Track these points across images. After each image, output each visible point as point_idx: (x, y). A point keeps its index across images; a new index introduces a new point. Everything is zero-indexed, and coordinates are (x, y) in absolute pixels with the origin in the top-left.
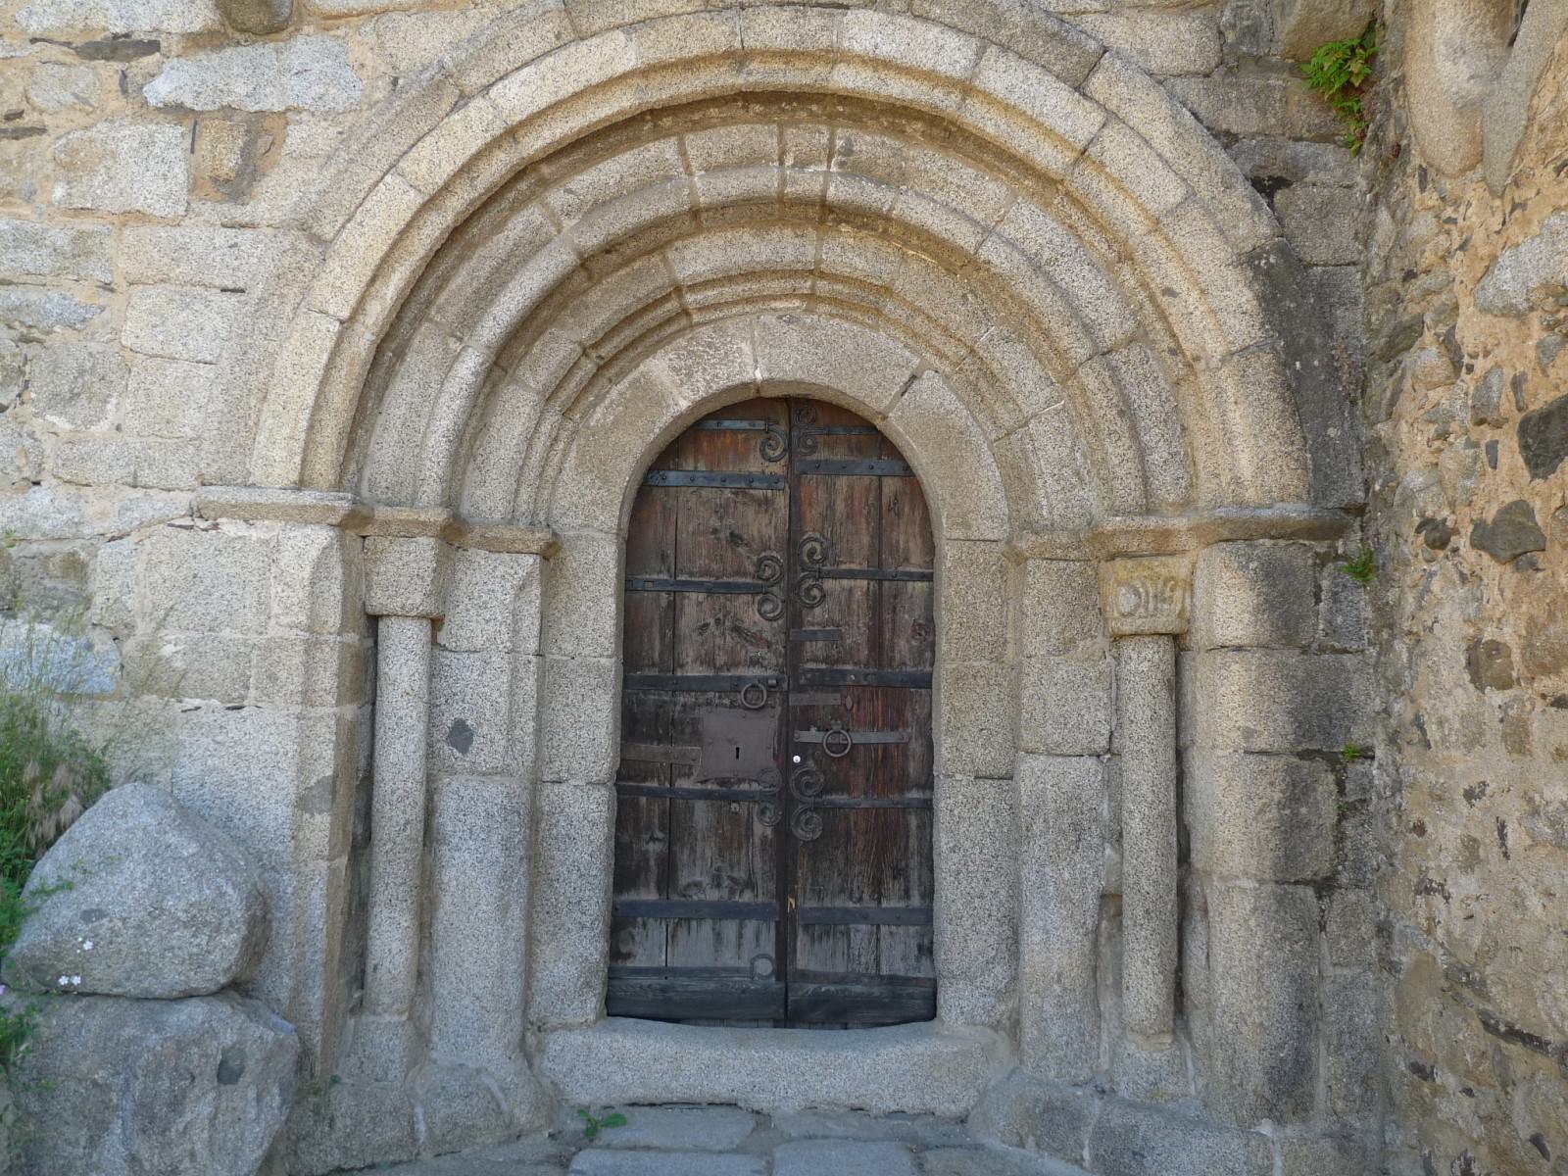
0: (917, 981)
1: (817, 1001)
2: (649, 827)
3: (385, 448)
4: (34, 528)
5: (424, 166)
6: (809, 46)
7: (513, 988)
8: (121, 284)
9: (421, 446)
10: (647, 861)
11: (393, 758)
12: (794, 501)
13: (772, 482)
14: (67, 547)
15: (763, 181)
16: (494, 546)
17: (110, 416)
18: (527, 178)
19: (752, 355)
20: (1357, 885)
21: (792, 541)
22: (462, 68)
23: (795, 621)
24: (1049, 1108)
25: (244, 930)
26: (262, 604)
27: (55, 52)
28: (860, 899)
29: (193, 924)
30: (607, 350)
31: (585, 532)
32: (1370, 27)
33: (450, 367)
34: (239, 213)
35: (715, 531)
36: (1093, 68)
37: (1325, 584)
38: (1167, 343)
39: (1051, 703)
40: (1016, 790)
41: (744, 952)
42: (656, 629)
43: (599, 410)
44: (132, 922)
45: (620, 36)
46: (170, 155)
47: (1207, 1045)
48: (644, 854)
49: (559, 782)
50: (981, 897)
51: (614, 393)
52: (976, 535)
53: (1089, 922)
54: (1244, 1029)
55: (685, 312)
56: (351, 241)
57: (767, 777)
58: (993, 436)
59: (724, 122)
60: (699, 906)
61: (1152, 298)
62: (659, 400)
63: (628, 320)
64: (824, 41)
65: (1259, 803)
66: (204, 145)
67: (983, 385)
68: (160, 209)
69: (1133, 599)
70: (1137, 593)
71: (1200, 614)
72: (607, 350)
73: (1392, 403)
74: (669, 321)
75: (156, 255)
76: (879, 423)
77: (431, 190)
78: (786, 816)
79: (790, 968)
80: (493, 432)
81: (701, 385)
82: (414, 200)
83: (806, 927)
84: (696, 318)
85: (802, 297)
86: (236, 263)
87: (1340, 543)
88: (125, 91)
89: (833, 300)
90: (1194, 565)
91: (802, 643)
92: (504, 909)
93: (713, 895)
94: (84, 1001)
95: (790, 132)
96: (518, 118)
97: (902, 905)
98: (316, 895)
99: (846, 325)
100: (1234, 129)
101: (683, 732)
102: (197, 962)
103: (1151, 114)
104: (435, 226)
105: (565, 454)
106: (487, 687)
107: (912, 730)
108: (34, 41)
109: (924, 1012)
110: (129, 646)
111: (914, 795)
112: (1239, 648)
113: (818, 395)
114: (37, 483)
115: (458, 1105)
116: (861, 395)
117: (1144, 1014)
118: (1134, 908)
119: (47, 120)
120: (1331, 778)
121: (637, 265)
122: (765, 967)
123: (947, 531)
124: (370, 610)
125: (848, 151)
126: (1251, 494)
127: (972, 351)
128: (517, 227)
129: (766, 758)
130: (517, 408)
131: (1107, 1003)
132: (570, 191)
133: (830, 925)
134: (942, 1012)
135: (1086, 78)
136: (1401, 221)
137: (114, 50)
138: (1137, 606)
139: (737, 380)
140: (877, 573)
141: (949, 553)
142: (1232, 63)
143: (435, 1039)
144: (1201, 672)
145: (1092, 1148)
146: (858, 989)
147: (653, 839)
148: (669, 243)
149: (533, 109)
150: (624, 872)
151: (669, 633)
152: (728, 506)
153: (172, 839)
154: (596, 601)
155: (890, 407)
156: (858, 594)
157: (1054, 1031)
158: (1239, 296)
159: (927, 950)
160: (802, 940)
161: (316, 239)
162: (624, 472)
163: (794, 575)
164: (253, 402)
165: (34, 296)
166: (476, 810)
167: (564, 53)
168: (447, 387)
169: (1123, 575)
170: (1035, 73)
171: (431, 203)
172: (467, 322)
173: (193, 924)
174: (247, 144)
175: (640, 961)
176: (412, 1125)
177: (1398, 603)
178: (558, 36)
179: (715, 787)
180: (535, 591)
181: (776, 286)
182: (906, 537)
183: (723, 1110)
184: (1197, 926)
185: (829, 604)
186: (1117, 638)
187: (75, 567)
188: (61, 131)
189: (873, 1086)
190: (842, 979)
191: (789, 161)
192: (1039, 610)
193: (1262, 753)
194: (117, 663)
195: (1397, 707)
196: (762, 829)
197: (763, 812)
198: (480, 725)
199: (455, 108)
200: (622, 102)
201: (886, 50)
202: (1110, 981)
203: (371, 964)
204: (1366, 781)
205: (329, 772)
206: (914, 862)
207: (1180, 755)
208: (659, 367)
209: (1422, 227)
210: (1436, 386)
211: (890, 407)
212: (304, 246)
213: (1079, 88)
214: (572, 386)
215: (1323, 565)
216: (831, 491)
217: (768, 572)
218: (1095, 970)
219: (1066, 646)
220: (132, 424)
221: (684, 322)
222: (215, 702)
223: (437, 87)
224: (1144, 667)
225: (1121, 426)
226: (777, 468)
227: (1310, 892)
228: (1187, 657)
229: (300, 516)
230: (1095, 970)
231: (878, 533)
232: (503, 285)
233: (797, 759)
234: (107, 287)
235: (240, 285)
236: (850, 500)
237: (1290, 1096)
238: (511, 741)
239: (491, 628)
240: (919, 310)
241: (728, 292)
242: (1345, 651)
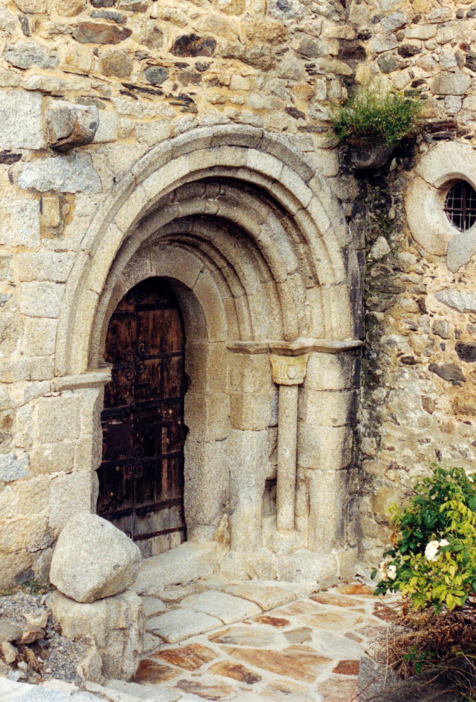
17: (18, 348)
32: (241, 59)
75: (31, 267)
81: (133, 280)
86: (62, 269)
99: (180, 250)
110: (32, 454)
112: (331, 390)
135: (309, 180)
144: (311, 396)
194: (27, 463)
213: (307, 182)
222: (62, 472)
235: (63, 280)
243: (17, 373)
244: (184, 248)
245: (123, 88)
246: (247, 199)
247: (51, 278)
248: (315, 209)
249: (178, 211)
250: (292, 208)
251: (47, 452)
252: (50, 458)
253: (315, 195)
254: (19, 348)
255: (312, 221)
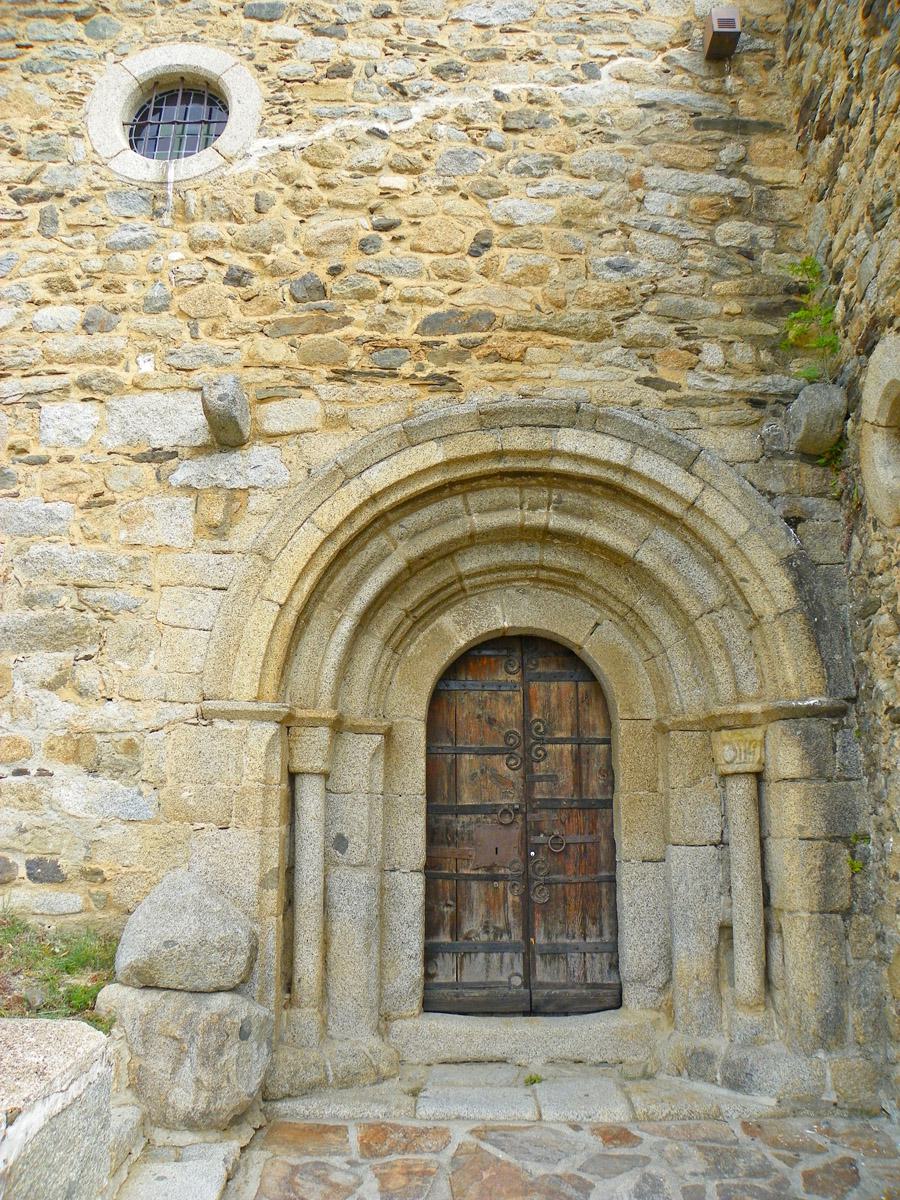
0: (609, 986)
1: (549, 1000)
2: (445, 898)
3: (300, 676)
4: (109, 725)
5: (326, 517)
6: (539, 448)
7: (374, 994)
8: (157, 587)
9: (319, 673)
10: (444, 918)
11: (307, 857)
12: (526, 698)
13: (513, 687)
14: (128, 736)
15: (512, 517)
16: (358, 730)
18: (382, 522)
19: (504, 613)
20: (864, 911)
21: (526, 723)
22: (347, 463)
23: (529, 770)
24: (695, 1053)
25: (248, 954)
26: (239, 769)
27: (120, 459)
28: (574, 937)
29: (222, 950)
30: (418, 613)
31: (406, 720)
32: (841, 438)
33: (335, 628)
34: (224, 546)
35: (479, 717)
36: (695, 459)
37: (838, 742)
38: (744, 607)
39: (687, 814)
40: (668, 868)
41: (506, 972)
42: (445, 777)
43: (413, 647)
44: (190, 948)
45: (433, 444)
46: (184, 514)
47: (785, 1010)
48: (442, 915)
49: (394, 870)
50: (648, 932)
51: (421, 637)
52: (637, 717)
53: (714, 943)
54: (806, 998)
55: (463, 590)
56: (285, 560)
57: (516, 866)
58: (646, 658)
59: (489, 487)
60: (475, 945)
61: (734, 583)
62: (448, 640)
63: (432, 596)
64: (547, 445)
65: (809, 868)
66: (202, 507)
67: (639, 629)
68: (179, 543)
69: (733, 753)
70: (735, 750)
71: (770, 761)
72: (418, 613)
73: (868, 643)
74: (453, 595)
76: (576, 651)
77: (330, 530)
78: (527, 889)
79: (532, 981)
80: (355, 663)
81: (473, 631)
82: (320, 536)
83: (541, 955)
84: (469, 593)
85: (531, 579)
87: (844, 719)
88: (159, 479)
89: (549, 582)
90: (765, 732)
91: (533, 782)
92: (368, 946)
93: (484, 938)
94: (164, 993)
95: (526, 491)
96: (378, 490)
97: (598, 940)
98: (271, 938)
100: (773, 490)
101: (463, 839)
102: (224, 971)
103: (728, 480)
104: (332, 549)
105: (393, 673)
106: (358, 817)
107: (601, 834)
108: (109, 454)
109: (614, 1004)
110: (163, 793)
111: (604, 873)
112: (793, 780)
113: (539, 634)
114: (110, 700)
115: (350, 1061)
116: (566, 635)
117: (748, 994)
118: (739, 933)
119: (118, 497)
120: (847, 851)
121: (437, 564)
122: (517, 981)
123: (620, 712)
124: (292, 770)
125: (559, 501)
126: (794, 692)
127: (631, 609)
128: (372, 548)
129: (515, 855)
130: (372, 646)
131: (726, 990)
132: (402, 526)
133: (555, 954)
134: (625, 1002)
136: (866, 546)
137: (154, 457)
138: (735, 758)
139: (494, 627)
140: (578, 739)
141: (622, 727)
142: (769, 454)
143: (330, 1024)
144: (772, 791)
145: (722, 1073)
146: (573, 992)
147: (448, 905)
148: (455, 551)
149: (386, 485)
150: (431, 928)
151: (453, 779)
152: (485, 702)
153: (207, 901)
154: (414, 760)
155: (584, 642)
156: (566, 753)
157: (696, 1008)
158: (781, 581)
159: (615, 966)
160: (539, 964)
161: (267, 560)
162: (428, 684)
163: (526, 744)
164: (231, 652)
165: (109, 593)
166: (354, 889)
167: (402, 454)
168: (334, 638)
169: (726, 738)
170: (664, 462)
171: (330, 538)
172: (344, 601)
173: (222, 950)
174: (227, 506)
175: (441, 979)
176: (326, 1071)
177: (878, 752)
178: (399, 445)
179: (484, 873)
180: (381, 756)
181: (516, 574)
182: (593, 716)
183: (498, 1065)
184: (776, 941)
185: (548, 759)
186: (724, 776)
187: (131, 747)
188: (123, 502)
189: (588, 1048)
190: (564, 986)
191: (526, 506)
192: (678, 760)
193: (808, 839)
195: (881, 810)
196: (512, 898)
197: (513, 886)
198: (352, 837)
199: (343, 484)
200: (436, 479)
201: (582, 450)
202: (726, 978)
203: (296, 978)
204: (866, 852)
205: (276, 865)
206: (605, 914)
207: (762, 841)
208: (447, 621)
209: (876, 549)
210: (889, 635)
211: (584, 642)
212: (260, 563)
213: (689, 469)
214: (399, 635)
215: (836, 731)
216: (548, 690)
217: (512, 741)
218: (717, 971)
219: (696, 780)
220: (163, 665)
221: (462, 595)
223: (333, 474)
224: (741, 792)
225: (721, 653)
226: (515, 678)
227: (839, 917)
228: (765, 787)
229: (260, 717)
230: (717, 971)
231: (577, 716)
232: (364, 579)
233: (533, 853)
234: (149, 588)
235: (224, 586)
236: (559, 694)
237: (834, 1034)
238: (371, 846)
239: (357, 779)
240: (600, 587)
241: (488, 578)
242: (851, 779)
243: (147, 690)
244: (557, 591)
245: (332, 375)
246: (607, 508)
247: (205, 583)
248: (711, 503)
249: (472, 522)
250: (672, 506)
251: (186, 795)
252: (191, 803)
253: (707, 485)
254: (152, 661)
255: (713, 522)
